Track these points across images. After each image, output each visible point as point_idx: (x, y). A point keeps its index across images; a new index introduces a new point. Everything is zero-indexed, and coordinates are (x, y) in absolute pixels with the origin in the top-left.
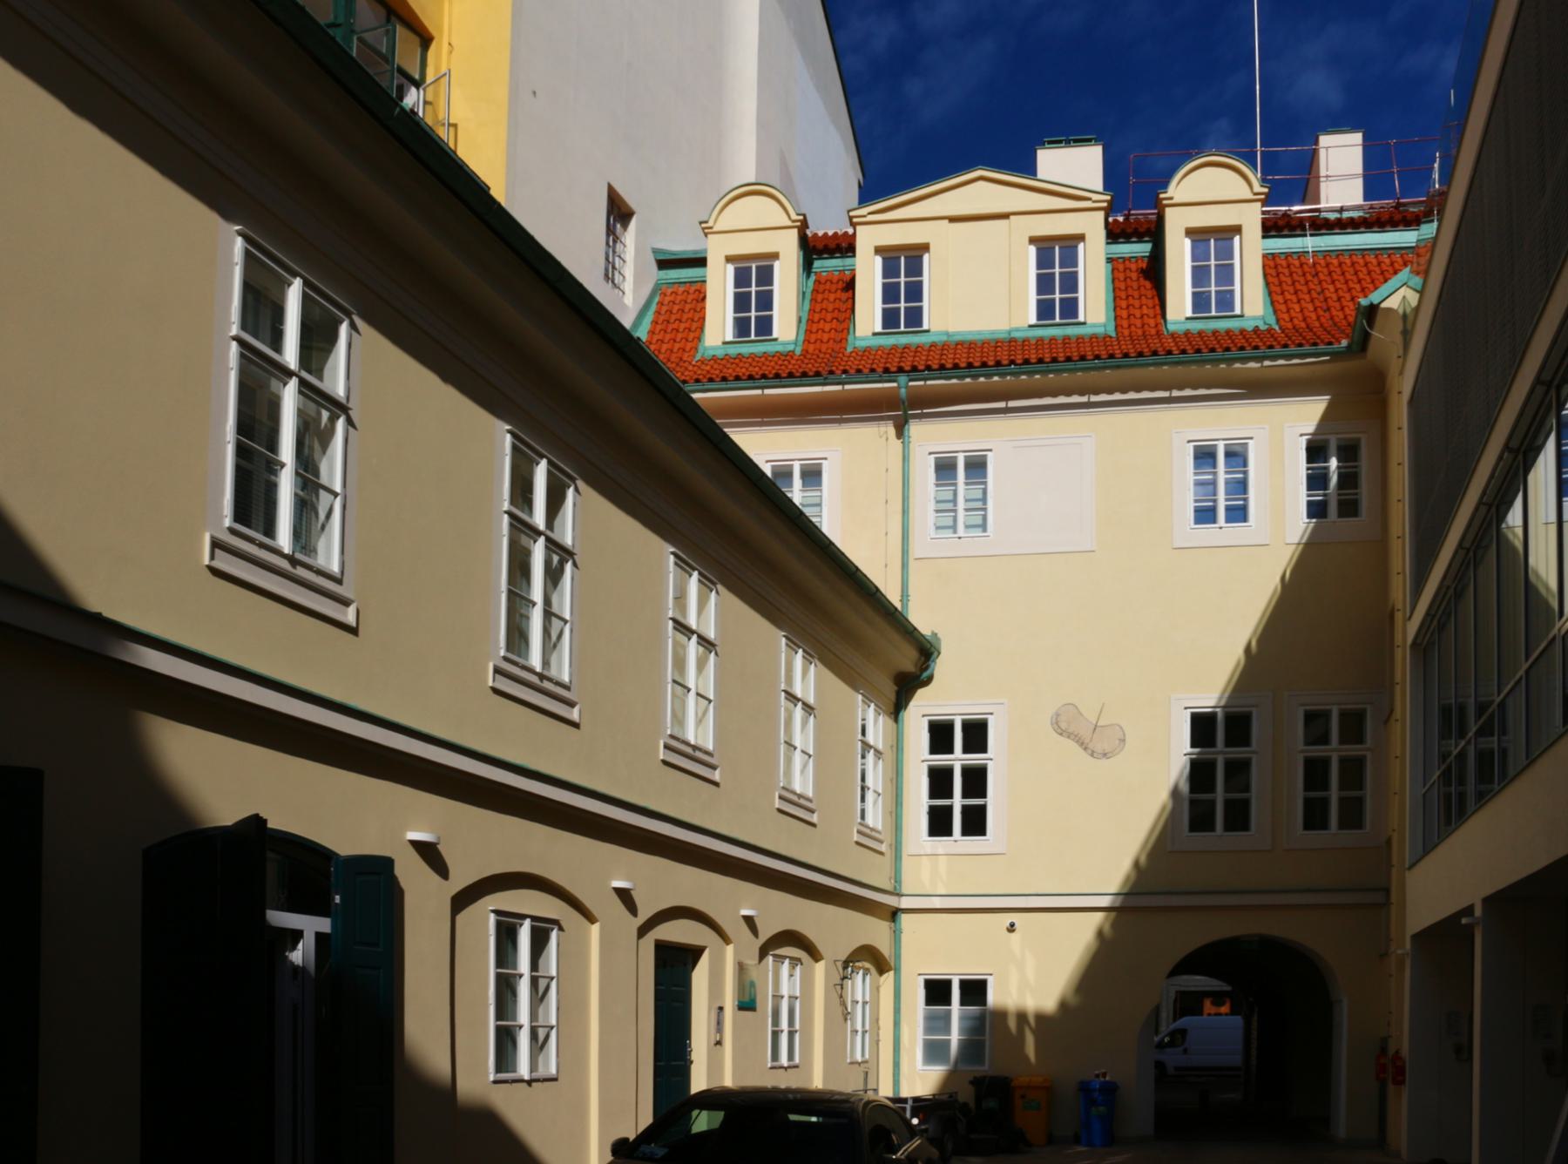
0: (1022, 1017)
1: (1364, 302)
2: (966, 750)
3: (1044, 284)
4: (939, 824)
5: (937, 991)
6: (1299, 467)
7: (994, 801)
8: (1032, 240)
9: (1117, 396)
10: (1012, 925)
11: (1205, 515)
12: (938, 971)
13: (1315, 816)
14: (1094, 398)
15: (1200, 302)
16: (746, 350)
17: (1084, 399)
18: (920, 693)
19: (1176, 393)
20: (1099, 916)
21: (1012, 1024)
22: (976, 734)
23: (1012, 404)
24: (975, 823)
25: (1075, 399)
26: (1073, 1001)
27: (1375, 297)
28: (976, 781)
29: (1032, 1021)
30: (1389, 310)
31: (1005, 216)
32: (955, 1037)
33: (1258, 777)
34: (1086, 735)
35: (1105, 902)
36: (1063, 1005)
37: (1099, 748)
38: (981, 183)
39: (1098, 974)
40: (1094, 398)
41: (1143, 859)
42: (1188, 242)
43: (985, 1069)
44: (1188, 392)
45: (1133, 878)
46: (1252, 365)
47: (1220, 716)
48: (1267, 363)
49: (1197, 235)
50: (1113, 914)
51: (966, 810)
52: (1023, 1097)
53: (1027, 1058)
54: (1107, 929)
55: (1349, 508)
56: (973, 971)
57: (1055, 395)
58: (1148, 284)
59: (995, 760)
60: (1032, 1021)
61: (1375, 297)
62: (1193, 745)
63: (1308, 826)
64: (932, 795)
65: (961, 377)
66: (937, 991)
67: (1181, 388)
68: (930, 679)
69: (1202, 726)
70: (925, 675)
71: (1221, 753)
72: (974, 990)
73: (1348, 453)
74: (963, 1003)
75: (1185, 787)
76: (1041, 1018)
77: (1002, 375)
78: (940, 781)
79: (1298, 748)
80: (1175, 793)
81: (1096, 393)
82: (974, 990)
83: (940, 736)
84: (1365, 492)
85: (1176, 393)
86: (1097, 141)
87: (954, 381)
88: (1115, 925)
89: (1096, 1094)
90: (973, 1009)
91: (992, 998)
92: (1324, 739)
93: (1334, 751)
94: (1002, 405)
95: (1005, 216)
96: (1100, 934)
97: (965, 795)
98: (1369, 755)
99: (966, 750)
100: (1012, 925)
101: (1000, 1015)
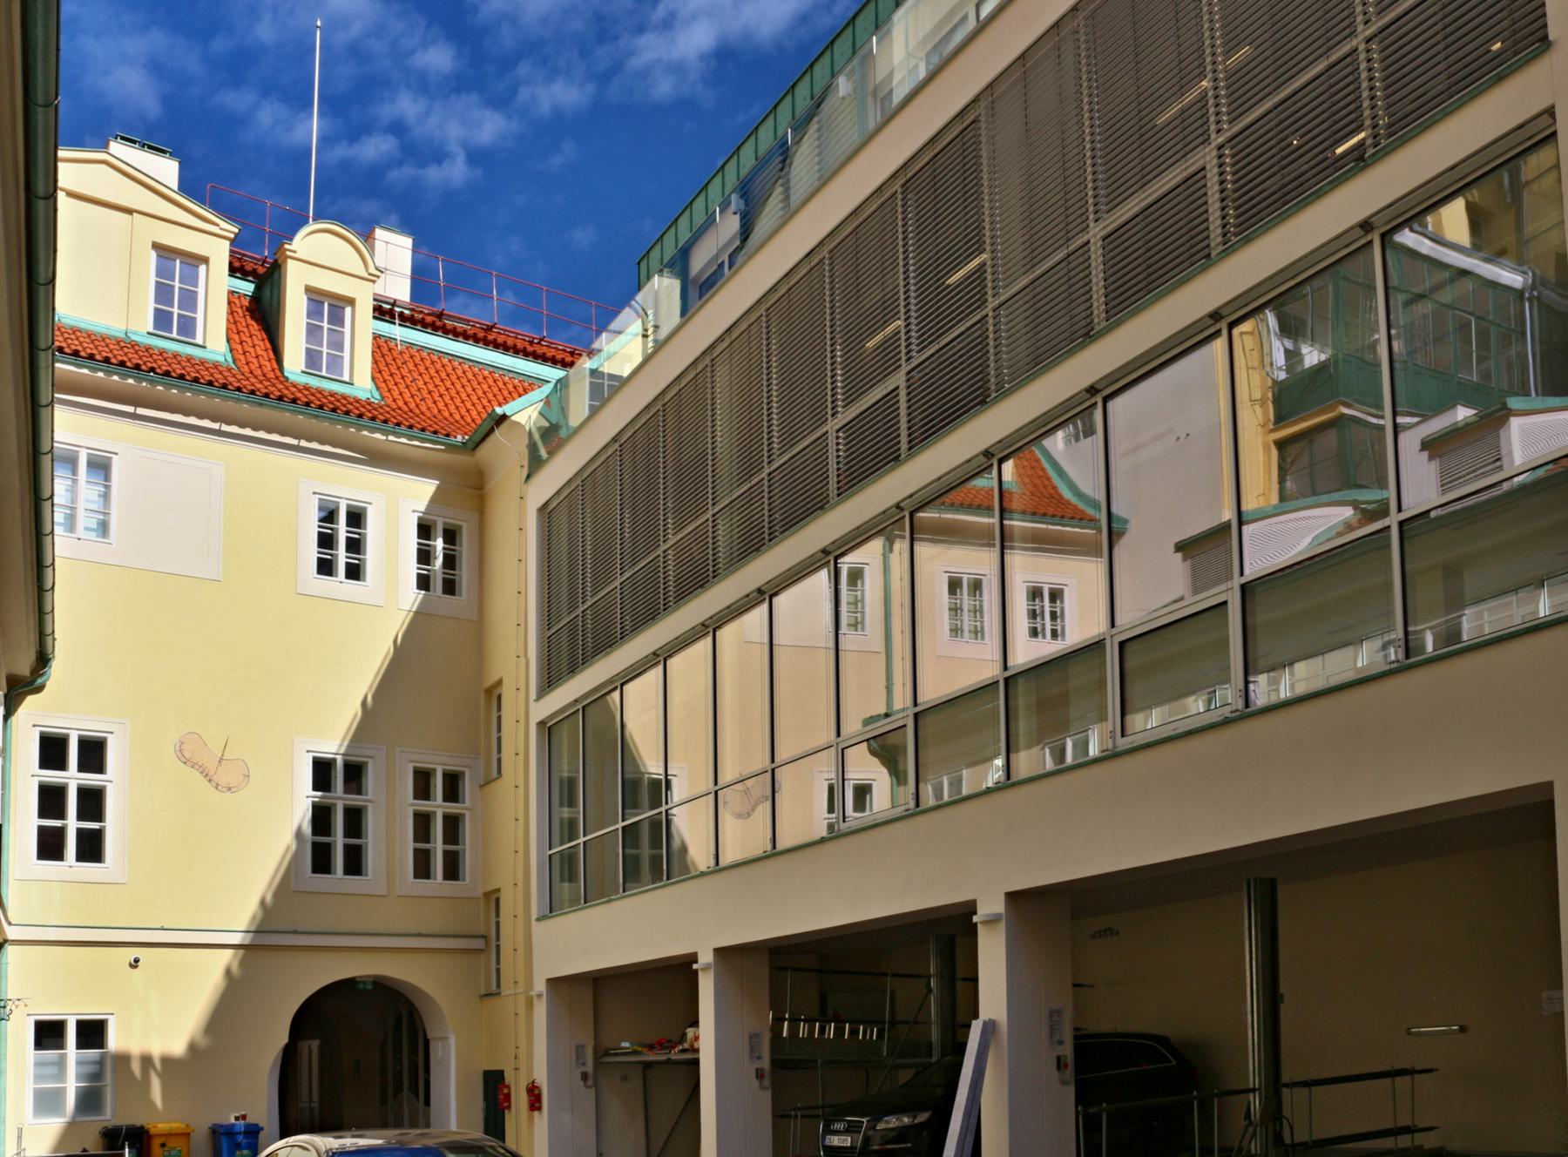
0: (146, 1060)
1: (499, 411)
2: (81, 768)
3: (163, 293)
4: (50, 846)
5: (48, 1034)
6: (411, 542)
7: (113, 825)
8: (156, 246)
9: (248, 432)
10: (137, 961)
11: (326, 567)
12: (50, 1013)
13: (422, 868)
14: (225, 428)
15: (312, 359)
16: (314, 382)
17: (216, 426)
18: (30, 699)
19: (303, 443)
20: (228, 954)
21: (136, 1068)
22: (93, 754)
23: (140, 411)
24: (91, 848)
25: (206, 423)
26: (203, 1042)
27: (507, 409)
28: (92, 802)
29: (158, 1064)
30: (517, 424)
31: (129, 211)
32: (72, 1086)
33: (372, 823)
34: (211, 768)
35: (236, 939)
36: (192, 1047)
37: (223, 781)
38: (104, 167)
39: (226, 1015)
40: (225, 428)
41: (269, 898)
42: (153, 254)
43: (110, 1116)
44: (315, 445)
45: (259, 916)
46: (378, 436)
47: (339, 759)
48: (391, 438)
49: (316, 297)
50: (241, 952)
51: (81, 833)
52: (163, 1145)
53: (152, 1104)
54: (235, 968)
55: (450, 587)
56: (92, 1012)
57: (187, 414)
58: (254, 327)
59: (114, 779)
60: (158, 1064)
61: (507, 409)
62: (315, 788)
63: (315, 870)
64: (43, 813)
65: (124, 377)
66: (48, 1034)
67: (309, 440)
68: (40, 689)
69: (322, 771)
70: (39, 681)
71: (340, 798)
72: (92, 1033)
73: (451, 536)
74: (80, 1045)
75: (307, 829)
76: (167, 1061)
77: (151, 382)
78: (51, 800)
79: (408, 805)
80: (299, 834)
81: (229, 424)
82: (92, 1033)
83: (52, 750)
84: (465, 574)
85: (303, 443)
86: (173, 155)
87: (85, 371)
88: (242, 963)
89: (240, 1138)
90: (93, 1053)
91: (115, 1041)
92: (61, 765)
93: (72, 778)
94: (130, 409)
95: (129, 211)
96: (228, 972)
97: (80, 817)
98: (468, 814)
99: (81, 768)
100: (137, 961)
101: (123, 1059)
